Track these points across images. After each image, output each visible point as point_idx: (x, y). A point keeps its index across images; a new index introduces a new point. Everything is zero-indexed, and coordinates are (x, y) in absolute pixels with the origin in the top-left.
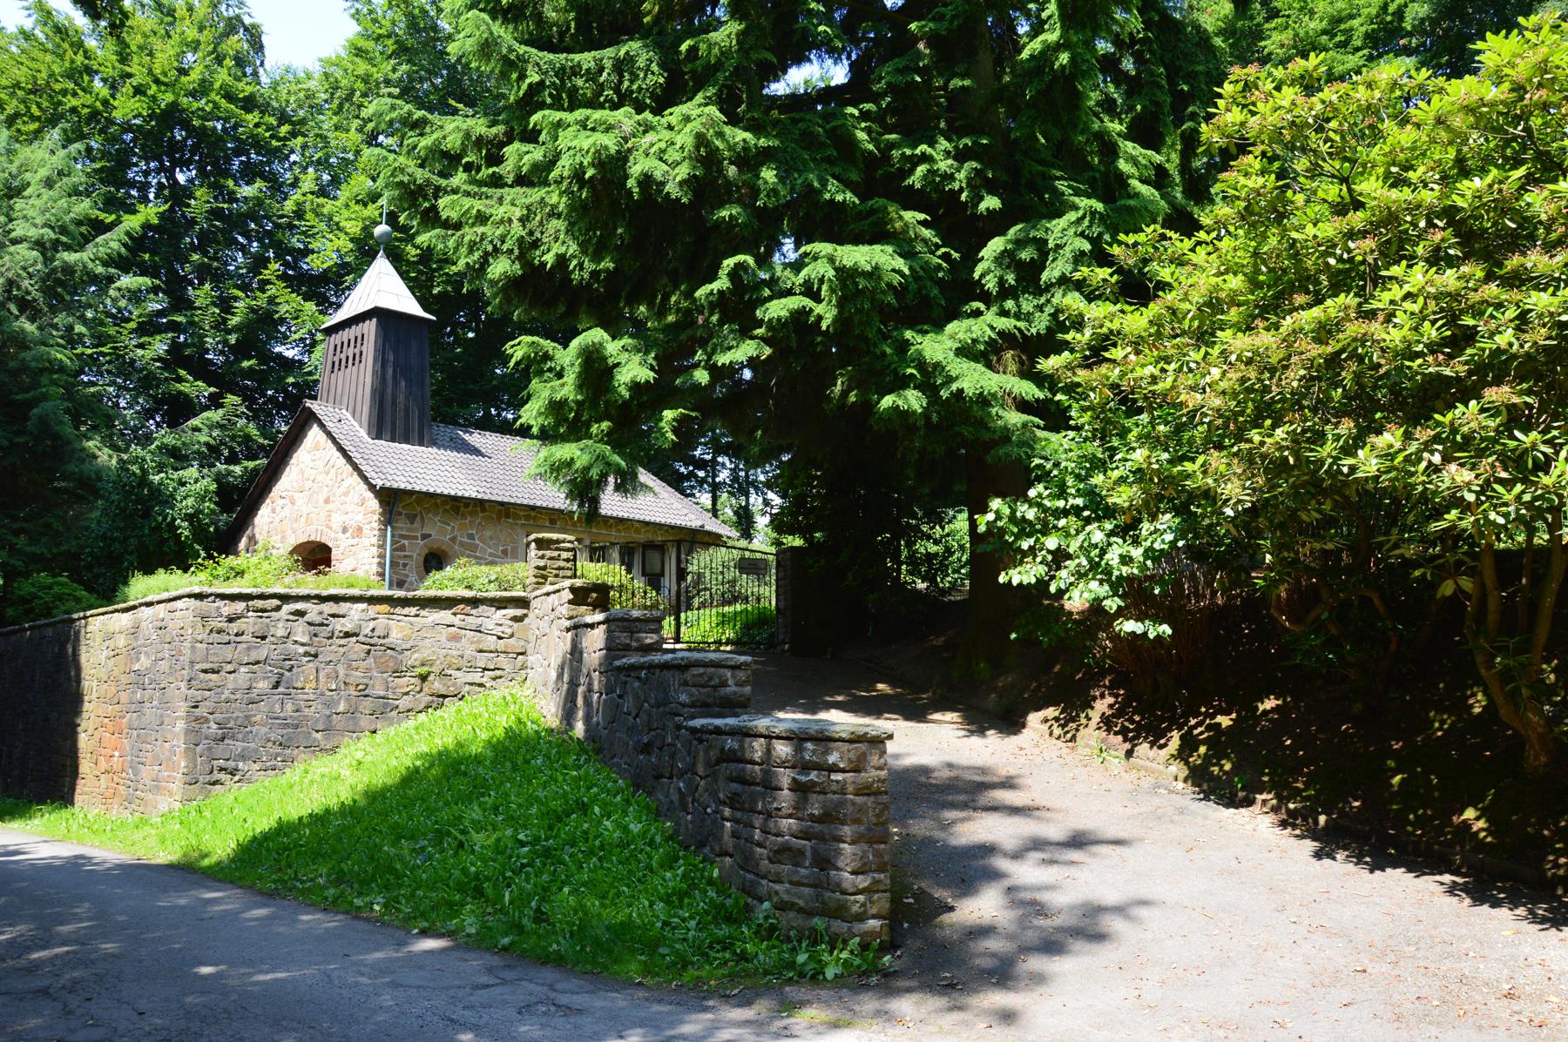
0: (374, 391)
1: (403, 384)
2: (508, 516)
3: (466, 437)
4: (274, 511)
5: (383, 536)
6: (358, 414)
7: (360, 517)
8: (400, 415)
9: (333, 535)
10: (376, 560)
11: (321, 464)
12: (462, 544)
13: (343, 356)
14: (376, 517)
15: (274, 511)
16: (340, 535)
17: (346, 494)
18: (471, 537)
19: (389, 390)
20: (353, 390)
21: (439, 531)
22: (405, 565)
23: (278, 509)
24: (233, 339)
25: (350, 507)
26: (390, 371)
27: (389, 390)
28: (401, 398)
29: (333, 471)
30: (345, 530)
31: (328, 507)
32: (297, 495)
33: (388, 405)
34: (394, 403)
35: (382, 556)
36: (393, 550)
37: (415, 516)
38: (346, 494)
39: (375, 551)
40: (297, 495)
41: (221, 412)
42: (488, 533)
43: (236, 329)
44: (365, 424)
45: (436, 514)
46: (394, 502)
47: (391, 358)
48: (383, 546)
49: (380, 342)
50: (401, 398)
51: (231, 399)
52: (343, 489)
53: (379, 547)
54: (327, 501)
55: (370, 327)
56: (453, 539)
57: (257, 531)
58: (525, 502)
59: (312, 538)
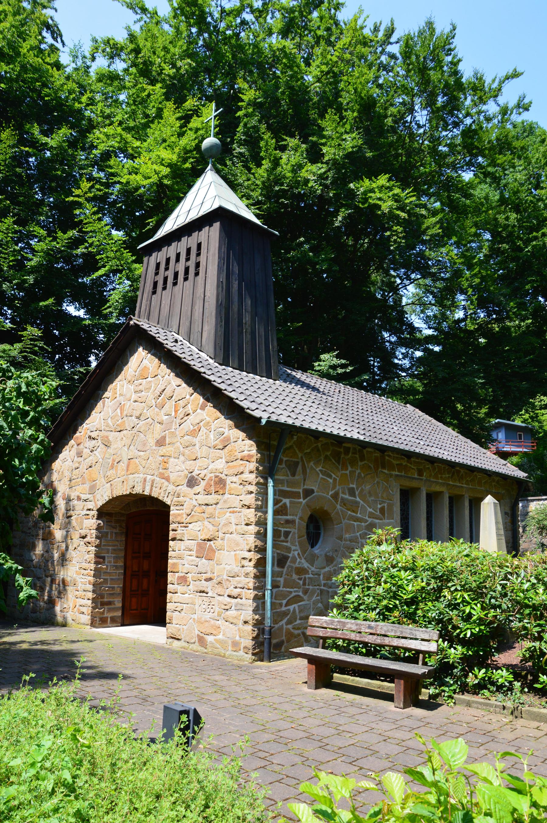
0: (219, 306)
1: (248, 302)
2: (383, 467)
3: (294, 373)
4: (79, 454)
5: (263, 493)
6: (195, 336)
7: (220, 465)
8: (247, 338)
9: (171, 488)
10: (253, 529)
11: (150, 396)
12: (344, 503)
13: (170, 274)
14: (253, 466)
15: (79, 454)
16: (184, 488)
17: (194, 433)
18: (352, 492)
19: (235, 307)
20: (187, 308)
21: (322, 483)
22: (287, 534)
23: (86, 451)
24: (31, 279)
25: (198, 451)
26: (235, 285)
27: (235, 307)
28: (247, 318)
29: (169, 406)
30: (192, 482)
31: (163, 450)
32: (112, 436)
33: (234, 324)
34: (240, 324)
35: (261, 523)
36: (276, 513)
37: (297, 464)
38: (194, 433)
39: (251, 514)
40: (112, 436)
41: (18, 346)
42: (368, 487)
43: (34, 270)
44: (210, 348)
45: (317, 463)
46: (278, 444)
47: (236, 270)
48: (262, 508)
49: (224, 249)
50: (247, 318)
51: (32, 331)
52: (188, 425)
53: (258, 509)
54: (161, 443)
55: (211, 235)
56: (335, 496)
57: (55, 477)
58: (402, 447)
59: (138, 490)
